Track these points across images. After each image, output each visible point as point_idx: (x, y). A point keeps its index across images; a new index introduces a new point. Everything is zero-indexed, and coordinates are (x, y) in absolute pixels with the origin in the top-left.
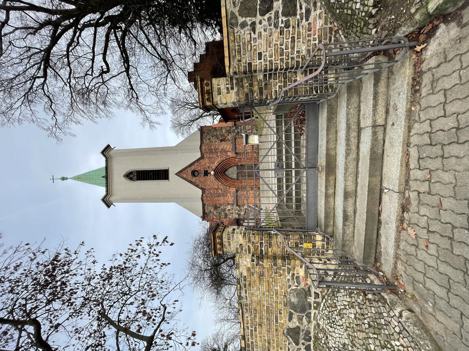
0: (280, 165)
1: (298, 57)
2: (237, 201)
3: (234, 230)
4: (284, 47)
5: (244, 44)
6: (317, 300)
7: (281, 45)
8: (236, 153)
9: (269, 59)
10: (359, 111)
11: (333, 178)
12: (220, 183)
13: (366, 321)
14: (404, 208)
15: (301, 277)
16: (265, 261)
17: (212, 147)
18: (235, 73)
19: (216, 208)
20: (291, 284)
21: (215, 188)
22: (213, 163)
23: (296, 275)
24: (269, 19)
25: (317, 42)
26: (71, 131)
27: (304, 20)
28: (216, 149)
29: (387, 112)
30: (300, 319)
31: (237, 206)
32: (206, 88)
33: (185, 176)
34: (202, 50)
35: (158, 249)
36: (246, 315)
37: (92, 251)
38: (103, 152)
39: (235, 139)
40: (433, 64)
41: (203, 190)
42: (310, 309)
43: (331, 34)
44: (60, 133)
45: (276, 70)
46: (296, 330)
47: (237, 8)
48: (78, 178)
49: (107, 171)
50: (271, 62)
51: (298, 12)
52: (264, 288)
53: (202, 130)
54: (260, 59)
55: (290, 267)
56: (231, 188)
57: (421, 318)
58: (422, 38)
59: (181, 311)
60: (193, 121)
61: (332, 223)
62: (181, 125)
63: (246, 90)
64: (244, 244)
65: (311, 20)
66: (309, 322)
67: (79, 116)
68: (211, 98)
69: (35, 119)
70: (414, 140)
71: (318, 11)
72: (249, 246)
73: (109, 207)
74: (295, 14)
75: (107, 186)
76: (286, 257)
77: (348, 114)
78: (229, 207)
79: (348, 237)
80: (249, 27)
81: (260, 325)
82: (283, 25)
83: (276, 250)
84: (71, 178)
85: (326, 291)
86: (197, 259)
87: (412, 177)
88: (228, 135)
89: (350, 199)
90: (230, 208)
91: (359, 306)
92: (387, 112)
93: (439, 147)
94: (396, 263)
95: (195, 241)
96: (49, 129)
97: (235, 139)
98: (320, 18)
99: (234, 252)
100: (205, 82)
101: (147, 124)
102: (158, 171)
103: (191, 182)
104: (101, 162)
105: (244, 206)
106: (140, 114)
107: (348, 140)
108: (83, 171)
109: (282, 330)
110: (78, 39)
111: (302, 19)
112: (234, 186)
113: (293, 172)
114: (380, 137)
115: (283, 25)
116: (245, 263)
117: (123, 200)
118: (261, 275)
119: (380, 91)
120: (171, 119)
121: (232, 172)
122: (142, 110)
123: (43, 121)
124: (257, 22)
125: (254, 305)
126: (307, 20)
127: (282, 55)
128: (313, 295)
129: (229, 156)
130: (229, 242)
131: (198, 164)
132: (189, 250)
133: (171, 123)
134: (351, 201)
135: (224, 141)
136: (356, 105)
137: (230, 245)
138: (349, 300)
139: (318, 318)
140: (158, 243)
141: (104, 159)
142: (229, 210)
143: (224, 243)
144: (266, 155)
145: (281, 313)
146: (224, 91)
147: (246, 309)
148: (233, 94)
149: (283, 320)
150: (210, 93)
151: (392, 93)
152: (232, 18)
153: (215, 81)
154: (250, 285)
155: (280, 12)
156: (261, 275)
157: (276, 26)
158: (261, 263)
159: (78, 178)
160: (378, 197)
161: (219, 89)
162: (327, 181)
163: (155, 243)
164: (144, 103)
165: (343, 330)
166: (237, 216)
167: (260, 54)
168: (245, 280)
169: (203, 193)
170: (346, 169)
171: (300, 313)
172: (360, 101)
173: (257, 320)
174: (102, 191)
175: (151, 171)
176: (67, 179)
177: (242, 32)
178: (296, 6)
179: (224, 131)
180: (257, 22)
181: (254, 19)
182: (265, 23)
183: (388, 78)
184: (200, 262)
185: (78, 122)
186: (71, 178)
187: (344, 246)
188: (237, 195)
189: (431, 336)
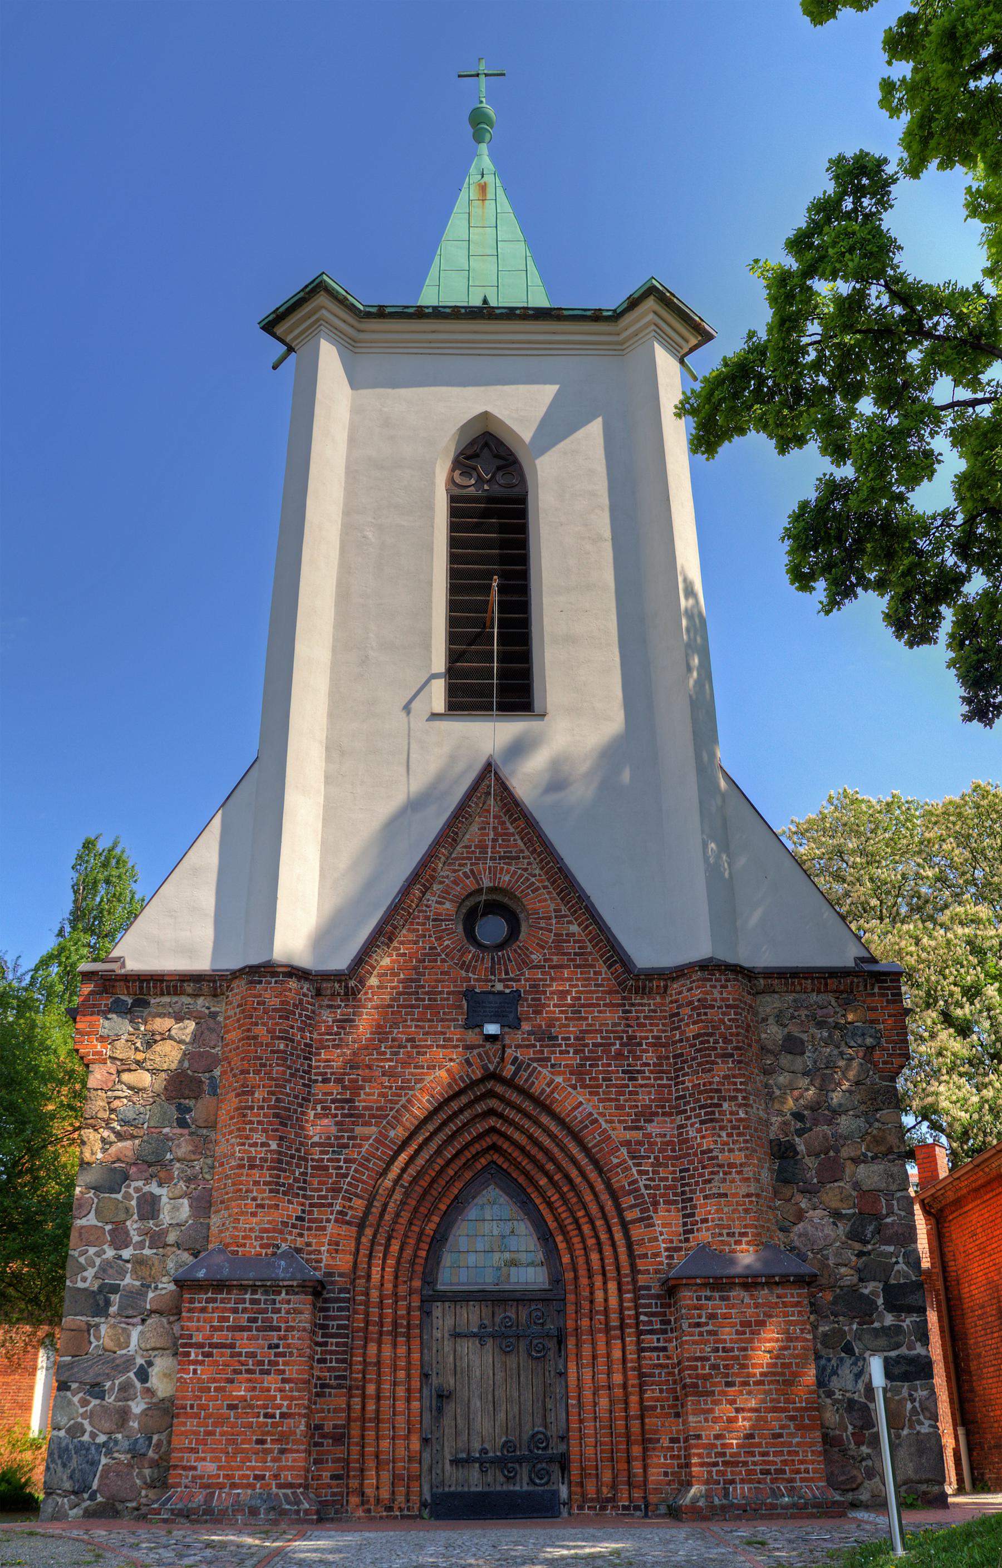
2: (220, 1286)
8: (671, 1289)
12: (398, 1133)
21: (356, 1089)
22: (579, 1073)
31: (184, 1284)
33: (472, 833)
73: (269, 326)
88: (836, 1215)
90: (166, 1217)
121: (493, 928)
129: (646, 1220)
131: (570, 947)
142: (149, 1207)
166: (86, 1280)
179: (871, 1175)
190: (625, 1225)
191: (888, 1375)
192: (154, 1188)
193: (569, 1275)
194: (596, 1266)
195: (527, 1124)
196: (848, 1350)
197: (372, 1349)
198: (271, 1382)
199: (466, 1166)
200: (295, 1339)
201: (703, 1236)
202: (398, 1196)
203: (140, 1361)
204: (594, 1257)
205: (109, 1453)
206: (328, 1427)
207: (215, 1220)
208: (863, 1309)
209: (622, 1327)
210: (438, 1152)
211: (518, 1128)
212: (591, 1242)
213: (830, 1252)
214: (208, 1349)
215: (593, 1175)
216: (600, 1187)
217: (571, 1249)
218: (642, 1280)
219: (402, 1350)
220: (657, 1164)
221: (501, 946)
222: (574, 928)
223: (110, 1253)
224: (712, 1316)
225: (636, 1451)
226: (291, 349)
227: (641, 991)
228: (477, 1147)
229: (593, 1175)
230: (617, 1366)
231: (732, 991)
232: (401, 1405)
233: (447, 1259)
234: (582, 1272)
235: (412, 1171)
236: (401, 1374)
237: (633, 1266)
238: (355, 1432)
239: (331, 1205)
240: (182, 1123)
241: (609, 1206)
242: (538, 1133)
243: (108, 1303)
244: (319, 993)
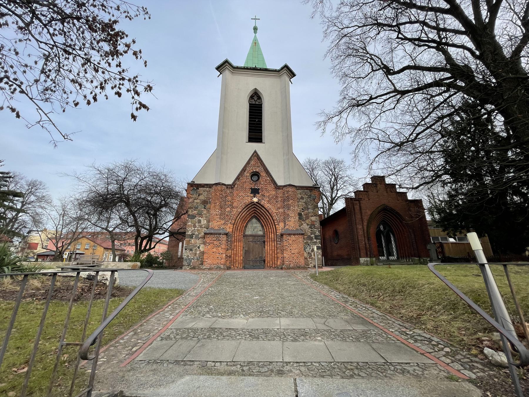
8: (282, 235)
12: (240, 210)
17: (291, 201)
19: (205, 203)
21: (233, 203)
22: (268, 201)
31: (205, 234)
33: (252, 162)
38: (286, 67)
39: (302, 234)
41: (231, 187)
48: (255, 43)
56: (231, 226)
67: (333, 37)
73: (218, 68)
75: (244, 68)
84: (255, 36)
86: (138, 176)
88: (308, 225)
90: (202, 223)
97: (302, 234)
101: (323, 119)
102: (261, 130)
103: (244, 170)
110: (424, 45)
112: (235, 229)
120: (318, 160)
121: (255, 178)
131: (268, 181)
132: (152, 166)
133: (315, 159)
135: (300, 218)
140: (138, 95)
141: (278, 68)
142: (199, 221)
166: (189, 233)
169: (227, 186)
175: (261, 121)
185: (326, 34)
186: (255, 36)
188: (220, 234)
190: (275, 225)
191: (317, 249)
192: (200, 218)
193: (266, 233)
194: (270, 231)
195: (260, 209)
196: (309, 245)
197: (235, 243)
198: (220, 248)
199: (250, 216)
200: (223, 242)
201: (287, 227)
202: (239, 220)
203: (198, 245)
204: (270, 230)
205: (193, 260)
206: (228, 255)
207: (210, 224)
208: (311, 239)
209: (274, 241)
210: (246, 213)
211: (259, 210)
212: (270, 228)
213: (307, 230)
214: (209, 244)
215: (270, 217)
216: (271, 219)
217: (266, 228)
218: (277, 234)
219: (240, 244)
220: (280, 216)
221: (257, 181)
222: (268, 178)
223: (193, 229)
224: (288, 239)
225: (276, 259)
226: (221, 74)
227: (279, 189)
228: (252, 213)
229: (270, 217)
230: (273, 246)
231: (294, 189)
232: (240, 252)
233: (247, 230)
234: (268, 232)
235: (242, 216)
236: (240, 247)
237: (276, 231)
238: (233, 256)
239: (80, 326)
240: (205, 208)
241: (273, 222)
242: (262, 211)
243: (193, 236)
244: (227, 188)
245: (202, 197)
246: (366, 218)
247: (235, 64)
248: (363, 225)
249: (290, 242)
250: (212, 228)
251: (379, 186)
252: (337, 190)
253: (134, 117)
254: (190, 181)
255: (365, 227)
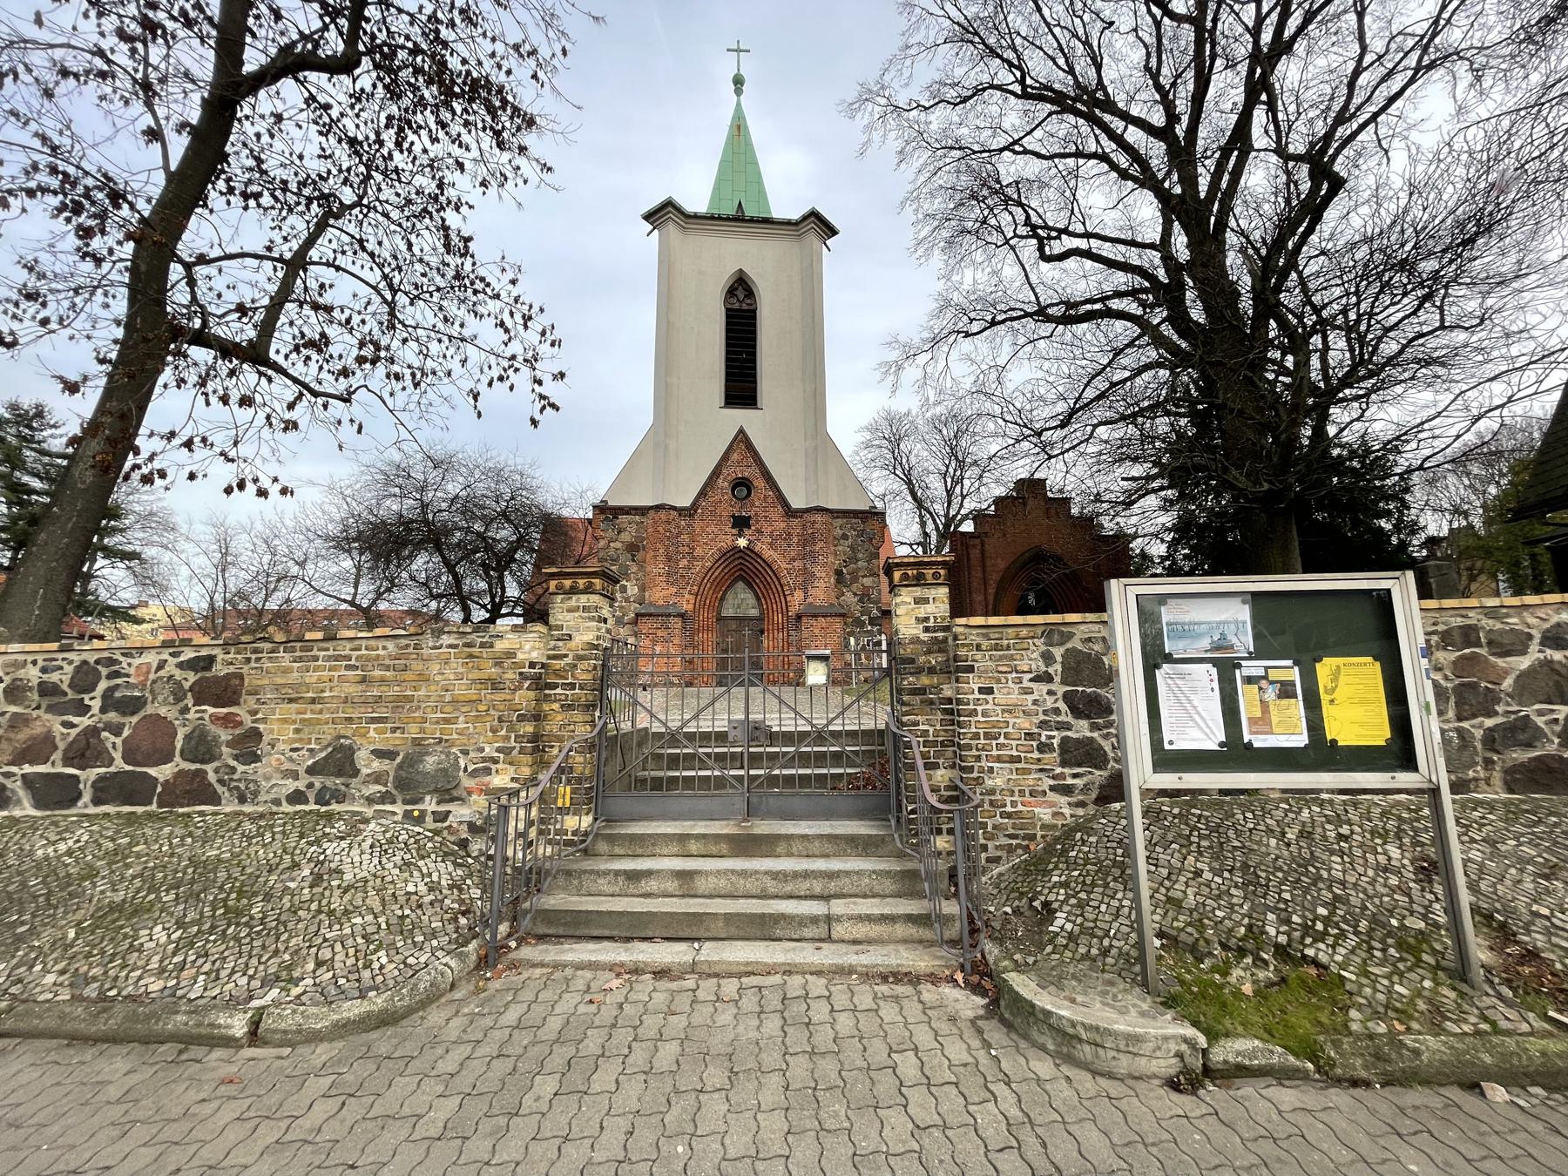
0: (758, 733)
1: (981, 770)
2: (650, 615)
3: (605, 621)
4: (1002, 740)
5: (1012, 658)
6: (429, 819)
7: (1007, 736)
8: (799, 617)
9: (979, 708)
10: (865, 896)
11: (725, 852)
12: (709, 564)
13: (407, 912)
14: (661, 973)
15: (488, 778)
16: (532, 694)
17: (820, 545)
18: (956, 638)
19: (633, 548)
20: (472, 755)
21: (693, 548)
22: (771, 544)
23: (493, 767)
24: (1057, 711)
25: (1009, 809)
26: (875, 145)
27: (1052, 782)
28: (813, 556)
29: (855, 942)
30: (377, 778)
31: (637, 615)
32: (929, 572)
33: (735, 456)
34: (1108, 525)
35: (522, 379)
36: (390, 645)
37: (520, 181)
38: (814, 215)
39: (843, 615)
40: (926, 996)
41: (689, 512)
42: (405, 802)
43: (1024, 838)
44: (871, 114)
45: (960, 725)
46: (348, 767)
47: (1080, 647)
48: (739, 127)
49: (758, 221)
50: (974, 713)
51: (1067, 771)
52: (461, 690)
53: (873, 517)
54: (981, 690)
55: (515, 752)
57: (443, 1000)
58: (975, 979)
59: (340, 447)
60: (909, 483)
61: (617, 850)
62: (895, 441)
63: (922, 659)
64: (572, 644)
65: (1052, 796)
66: (370, 800)
67: (921, 161)
68: (908, 582)
69: (913, 51)
70: (796, 980)
71: (1067, 811)
72: (566, 656)
73: (648, 217)
74: (1064, 764)
76: (538, 745)
77: (858, 873)
78: (633, 590)
79: (588, 883)
80: (1043, 668)
81: (363, 680)
82: (1043, 739)
83: (556, 719)
84: (739, 104)
85: (452, 839)
86: (461, 479)
87: (724, 982)
89: (676, 884)
90: (629, 592)
91: (436, 900)
92: (855, 942)
93: (780, 1007)
94: (543, 965)
95: (522, 475)
96: (883, 88)
97: (843, 615)
98: (1055, 814)
99: (552, 621)
100: (942, 572)
101: (894, 355)
102: (755, 375)
103: (716, 473)
104: (785, 206)
105: (636, 635)
106: (926, 335)
107: (806, 875)
108: (757, 131)
109: (349, 733)
111: (1054, 778)
113: (741, 772)
114: (808, 932)
115: (1043, 739)
116: (527, 647)
117: (663, 243)
118: (495, 685)
119: (897, 926)
121: (741, 602)
122: (936, 341)
123: (906, 73)
124: (1053, 687)
125: (417, 666)
126: (1052, 788)
127: (987, 736)
128: (443, 808)
130: (576, 609)
132: (494, 453)
133: (904, 411)
134: (671, 885)
136: (877, 889)
137: (570, 610)
138: (444, 883)
139: (383, 821)
143: (574, 598)
144: (781, 701)
145: (394, 730)
146: (922, 611)
147: (407, 646)
148: (914, 632)
149: (376, 737)
150: (919, 581)
151: (892, 947)
152: (1062, 634)
153: (943, 592)
154: (471, 656)
155: (1069, 734)
156: (495, 685)
157: (1043, 725)
158: (526, 684)
159: (739, 127)
160: (681, 934)
161: (926, 601)
162: (718, 838)
163: (539, 374)
164: (954, 354)
165: (372, 869)
167: (990, 691)
168: (482, 645)
169: (680, 511)
170: (744, 874)
171: (396, 777)
172: (884, 896)
173: (377, 673)
174: (697, 200)
176: (738, 92)
177: (1035, 655)
178: (1079, 765)
179: (868, 581)
180: (1053, 687)
181: (1057, 679)
182: (1050, 702)
183: (920, 942)
184: (450, 487)
186: (739, 104)
187: (569, 873)
189: (417, 1010)
201: (810, 600)
208: (862, 624)
245: (625, 537)
246: (994, 579)
247: (690, 208)
248: (985, 595)
249: (816, 631)
250: (651, 604)
251: (1031, 503)
252: (963, 497)
253: (534, 422)
254: (597, 502)
255: (991, 598)
